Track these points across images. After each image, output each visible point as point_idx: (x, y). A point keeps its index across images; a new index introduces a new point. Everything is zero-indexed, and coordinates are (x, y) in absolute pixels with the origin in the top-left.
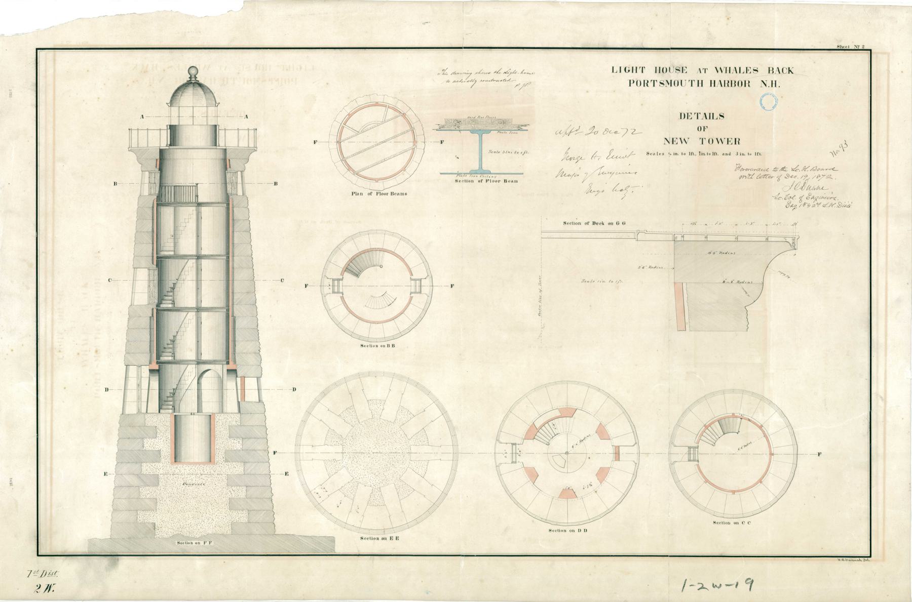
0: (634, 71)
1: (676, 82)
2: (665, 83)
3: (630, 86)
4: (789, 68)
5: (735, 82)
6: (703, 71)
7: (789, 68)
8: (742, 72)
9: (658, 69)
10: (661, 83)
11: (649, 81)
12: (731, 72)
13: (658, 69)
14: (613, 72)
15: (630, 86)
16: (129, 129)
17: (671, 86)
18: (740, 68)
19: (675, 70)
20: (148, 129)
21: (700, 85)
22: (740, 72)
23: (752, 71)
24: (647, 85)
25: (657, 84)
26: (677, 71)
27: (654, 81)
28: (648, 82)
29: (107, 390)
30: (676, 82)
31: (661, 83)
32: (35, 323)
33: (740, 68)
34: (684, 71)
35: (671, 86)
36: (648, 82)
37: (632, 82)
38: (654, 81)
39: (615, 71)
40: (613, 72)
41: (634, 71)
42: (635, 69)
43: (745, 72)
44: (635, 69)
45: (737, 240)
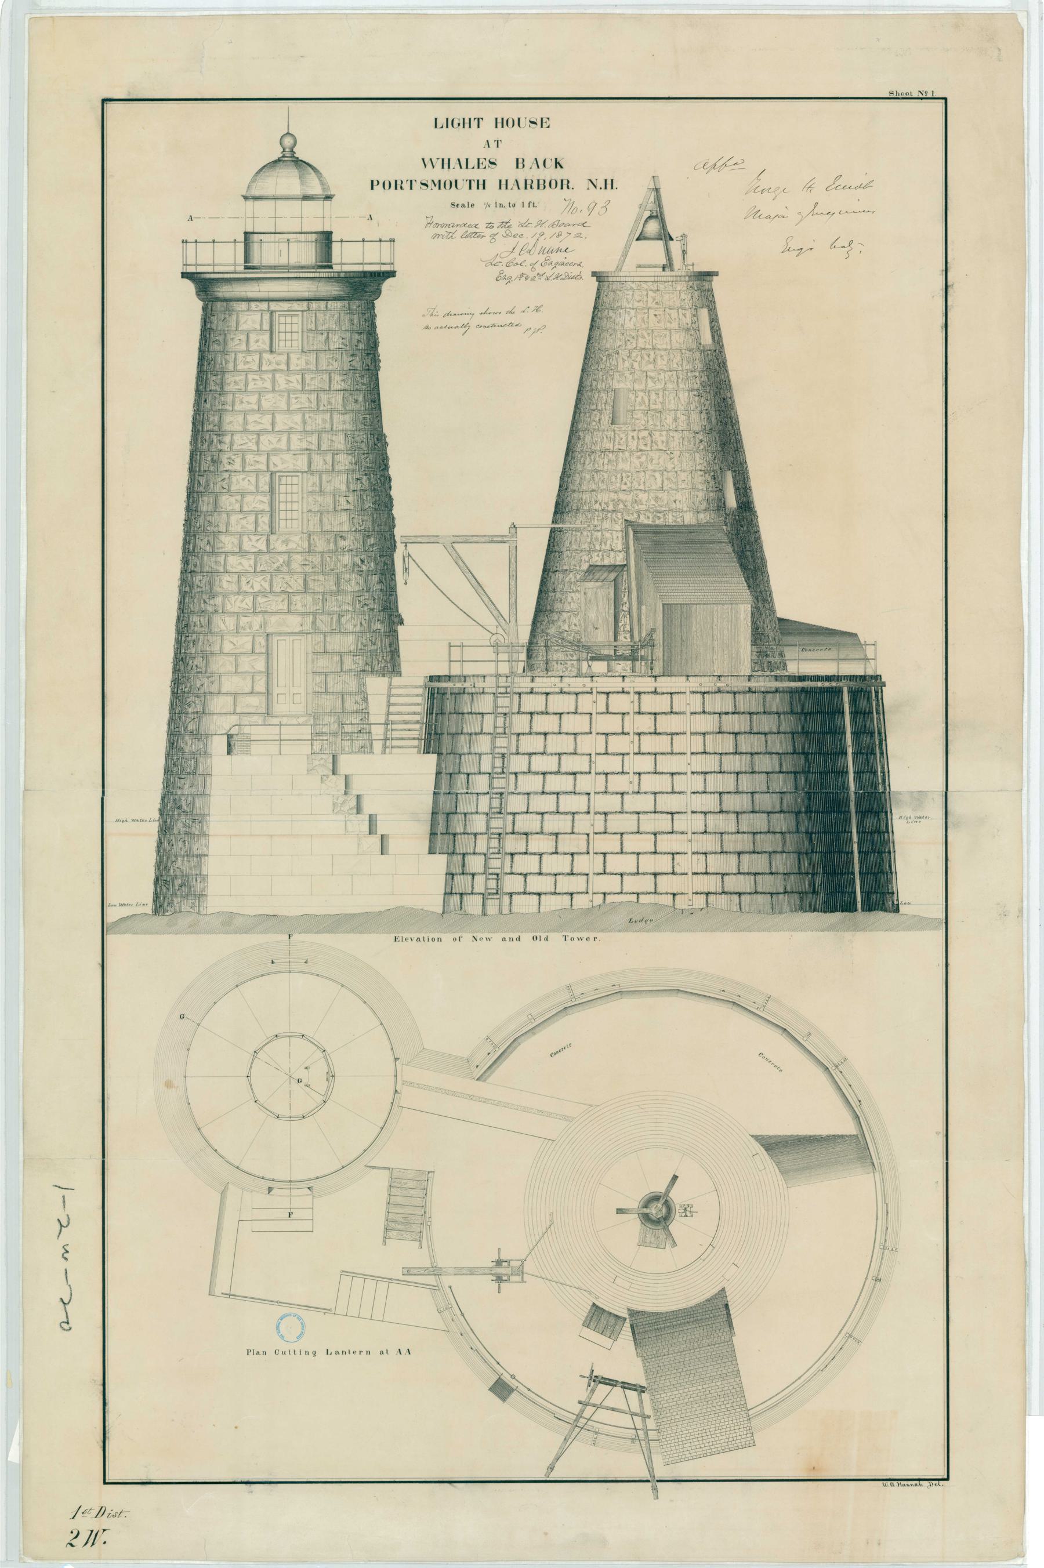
0: (467, 125)
1: (448, 186)
2: (430, 183)
3: (372, 189)
4: (556, 159)
5: (544, 181)
6: (493, 144)
7: (556, 159)
8: (470, 166)
9: (499, 121)
10: (422, 184)
11: (404, 182)
12: (452, 166)
13: (499, 121)
14: (436, 127)
15: (372, 189)
16: (896, 1251)
17: (440, 188)
18: (467, 160)
19: (528, 123)
20: (342, 241)
21: (503, 182)
22: (467, 168)
23: (487, 163)
24: (401, 188)
25: (416, 186)
26: (533, 125)
27: (411, 181)
28: (402, 182)
29: (182, 1017)
30: (448, 186)
31: (422, 184)
32: (101, 1104)
33: (467, 160)
34: (544, 124)
35: (440, 188)
36: (402, 182)
37: (375, 183)
38: (411, 181)
39: (439, 125)
40: (436, 127)
41: (467, 125)
42: (467, 121)
43: (476, 167)
44: (467, 121)
45: (689, 704)
